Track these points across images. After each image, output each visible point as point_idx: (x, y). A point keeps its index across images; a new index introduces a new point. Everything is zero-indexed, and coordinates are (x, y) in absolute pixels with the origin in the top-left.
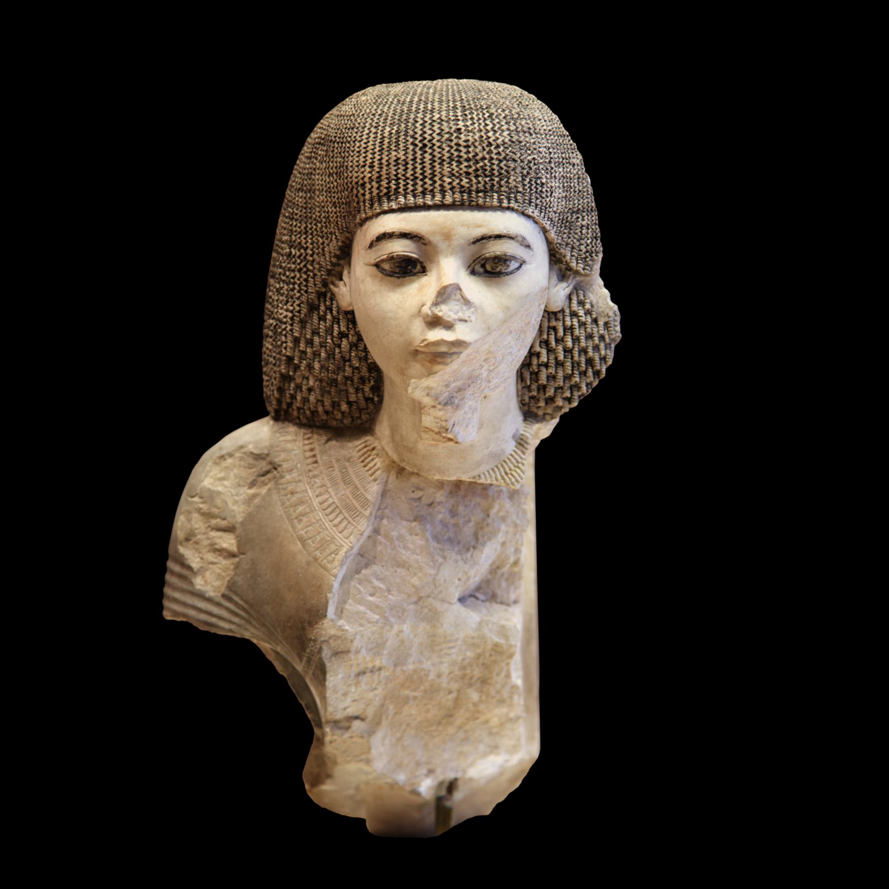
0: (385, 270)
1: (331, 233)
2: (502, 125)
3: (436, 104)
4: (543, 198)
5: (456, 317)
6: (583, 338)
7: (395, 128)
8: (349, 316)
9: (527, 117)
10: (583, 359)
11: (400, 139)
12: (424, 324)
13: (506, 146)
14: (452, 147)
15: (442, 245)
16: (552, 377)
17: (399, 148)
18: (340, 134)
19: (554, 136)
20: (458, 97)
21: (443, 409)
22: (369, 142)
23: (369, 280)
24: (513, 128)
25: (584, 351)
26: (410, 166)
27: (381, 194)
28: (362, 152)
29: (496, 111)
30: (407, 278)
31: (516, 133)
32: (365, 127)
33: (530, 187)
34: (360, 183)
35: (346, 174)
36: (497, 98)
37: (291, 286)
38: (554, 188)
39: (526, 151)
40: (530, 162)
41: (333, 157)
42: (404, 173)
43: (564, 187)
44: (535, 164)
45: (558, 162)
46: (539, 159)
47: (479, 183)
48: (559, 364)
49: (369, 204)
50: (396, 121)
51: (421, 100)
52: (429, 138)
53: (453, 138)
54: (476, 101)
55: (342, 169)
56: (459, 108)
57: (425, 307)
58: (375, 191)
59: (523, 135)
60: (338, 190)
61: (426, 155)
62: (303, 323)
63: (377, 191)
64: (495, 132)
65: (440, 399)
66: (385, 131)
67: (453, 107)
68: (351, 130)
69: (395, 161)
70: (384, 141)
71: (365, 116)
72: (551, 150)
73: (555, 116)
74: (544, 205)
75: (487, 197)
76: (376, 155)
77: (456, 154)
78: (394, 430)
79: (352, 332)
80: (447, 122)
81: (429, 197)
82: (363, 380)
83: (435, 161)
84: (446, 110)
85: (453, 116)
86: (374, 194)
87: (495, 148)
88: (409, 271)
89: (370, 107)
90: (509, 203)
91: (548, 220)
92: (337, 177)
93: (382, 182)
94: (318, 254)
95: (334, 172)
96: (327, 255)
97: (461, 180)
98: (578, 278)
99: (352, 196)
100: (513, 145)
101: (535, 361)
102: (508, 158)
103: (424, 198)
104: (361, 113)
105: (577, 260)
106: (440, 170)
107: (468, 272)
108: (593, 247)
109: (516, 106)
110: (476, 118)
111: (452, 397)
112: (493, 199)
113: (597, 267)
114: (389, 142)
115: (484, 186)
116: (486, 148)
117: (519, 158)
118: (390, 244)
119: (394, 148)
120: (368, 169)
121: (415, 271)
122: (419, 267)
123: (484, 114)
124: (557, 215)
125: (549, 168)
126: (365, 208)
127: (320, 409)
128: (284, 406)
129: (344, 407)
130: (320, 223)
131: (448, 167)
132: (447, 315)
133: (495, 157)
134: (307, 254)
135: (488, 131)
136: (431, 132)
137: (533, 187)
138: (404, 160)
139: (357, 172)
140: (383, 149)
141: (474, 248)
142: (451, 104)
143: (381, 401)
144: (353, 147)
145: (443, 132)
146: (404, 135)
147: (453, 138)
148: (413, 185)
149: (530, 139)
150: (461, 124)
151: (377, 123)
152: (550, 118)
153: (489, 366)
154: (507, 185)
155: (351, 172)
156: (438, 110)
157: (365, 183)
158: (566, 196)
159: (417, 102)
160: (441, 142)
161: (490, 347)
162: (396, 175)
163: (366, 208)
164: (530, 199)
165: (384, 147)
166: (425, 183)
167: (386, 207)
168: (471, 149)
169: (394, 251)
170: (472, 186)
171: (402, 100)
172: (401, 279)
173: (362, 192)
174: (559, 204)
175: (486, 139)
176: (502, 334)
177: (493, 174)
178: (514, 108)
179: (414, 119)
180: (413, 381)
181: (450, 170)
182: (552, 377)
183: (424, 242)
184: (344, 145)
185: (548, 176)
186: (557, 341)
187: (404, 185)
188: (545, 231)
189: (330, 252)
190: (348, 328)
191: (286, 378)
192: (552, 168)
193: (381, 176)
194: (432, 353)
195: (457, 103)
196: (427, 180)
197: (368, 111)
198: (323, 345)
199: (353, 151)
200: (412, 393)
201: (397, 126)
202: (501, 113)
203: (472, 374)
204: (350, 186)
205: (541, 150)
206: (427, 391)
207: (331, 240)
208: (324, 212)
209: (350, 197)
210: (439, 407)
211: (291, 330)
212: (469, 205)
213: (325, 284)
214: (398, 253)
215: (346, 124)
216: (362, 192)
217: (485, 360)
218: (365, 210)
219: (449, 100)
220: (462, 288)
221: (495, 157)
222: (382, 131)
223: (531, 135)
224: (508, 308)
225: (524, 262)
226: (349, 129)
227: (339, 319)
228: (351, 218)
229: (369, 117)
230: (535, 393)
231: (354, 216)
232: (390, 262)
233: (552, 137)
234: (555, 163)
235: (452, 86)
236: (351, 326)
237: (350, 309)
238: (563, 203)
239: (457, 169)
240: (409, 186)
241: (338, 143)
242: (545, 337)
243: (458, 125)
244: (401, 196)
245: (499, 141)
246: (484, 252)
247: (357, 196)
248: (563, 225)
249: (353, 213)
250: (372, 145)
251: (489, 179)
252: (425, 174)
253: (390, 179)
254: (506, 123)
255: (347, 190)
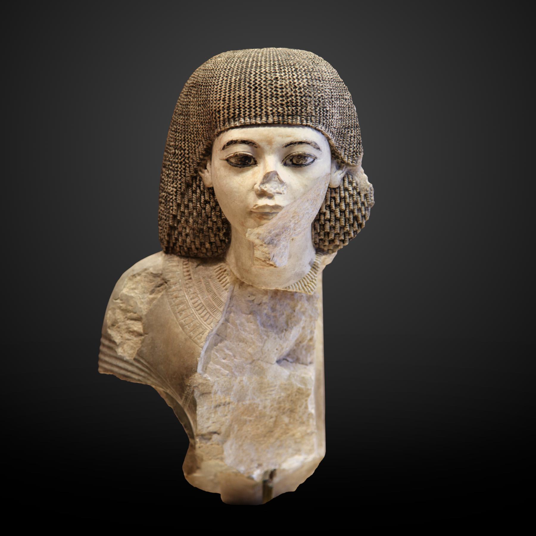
0: (232, 163)
1: (200, 141)
2: (303, 76)
3: (263, 63)
4: (328, 119)
5: (275, 191)
6: (351, 204)
7: (238, 77)
8: (211, 191)
9: (318, 70)
10: (352, 217)
11: (241, 84)
12: (255, 196)
13: (305, 88)
14: (272, 89)
15: (267, 148)
16: (333, 228)
17: (241, 89)
18: (205, 81)
19: (334, 82)
20: (276, 59)
21: (267, 247)
22: (222, 86)
23: (222, 169)
24: (309, 77)
25: (352, 212)
26: (247, 100)
27: (230, 117)
28: (218, 92)
29: (299, 67)
30: (246, 168)
31: (311, 80)
32: (220, 76)
33: (319, 113)
34: (217, 110)
35: (208, 105)
36: (300, 59)
37: (176, 173)
38: (334, 114)
39: (317, 91)
40: (319, 98)
41: (201, 95)
42: (243, 104)
43: (340, 113)
44: (322, 99)
45: (337, 98)
46: (325, 96)
47: (289, 110)
48: (337, 219)
49: (222, 123)
50: (239, 73)
51: (254, 60)
52: (259, 83)
53: (273, 83)
54: (287, 61)
55: (206, 102)
56: (277, 65)
57: (256, 185)
58: (226, 115)
59: (315, 81)
60: (204, 115)
61: (257, 94)
62: (183, 195)
63: (227, 115)
64: (299, 79)
65: (266, 241)
66: (232, 79)
67: (273, 65)
68: (211, 78)
69: (238, 97)
70: (231, 85)
71: (220, 70)
72: (332, 91)
73: (334, 70)
74: (328, 123)
75: (294, 119)
76: (227, 94)
77: (275, 93)
78: (238, 259)
79: (212, 200)
80: (269, 73)
81: (258, 119)
82: (219, 229)
83: (262, 97)
84: (269, 66)
85: (273, 70)
86: (226, 117)
87: (299, 89)
88: (246, 164)
89: (223, 65)
90: (307, 122)
91: (330, 133)
92: (203, 107)
93: (231, 110)
94: (192, 153)
95: (201, 104)
96: (197, 154)
97: (278, 109)
98: (349, 168)
99: (212, 118)
100: (309, 87)
101: (322, 218)
102: (306, 95)
103: (255, 119)
104: (218, 68)
105: (348, 157)
106: (265, 102)
107: (282, 164)
108: (357, 149)
109: (311, 64)
110: (287, 71)
111: (273, 239)
112: (297, 120)
113: (360, 161)
114: (234, 86)
115: (292, 112)
116: (293, 89)
117: (313, 95)
118: (235, 147)
119: (238, 89)
120: (222, 102)
121: (250, 164)
122: (252, 161)
123: (292, 69)
124: (336, 129)
125: (331, 101)
126: (220, 125)
127: (193, 247)
128: (171, 245)
129: (208, 245)
130: (193, 134)
131: (270, 101)
132: (269, 190)
133: (298, 95)
134: (185, 153)
135: (294, 79)
136: (260, 80)
137: (321, 113)
138: (244, 96)
139: (215, 104)
140: (231, 90)
141: (286, 149)
142: (272, 63)
143: (230, 242)
144: (213, 89)
145: (267, 80)
146: (243, 81)
147: (273, 83)
148: (249, 112)
149: (319, 84)
150: (278, 75)
151: (227, 74)
152: (332, 71)
153: (295, 221)
154: (305, 111)
155: (212, 104)
156: (264, 66)
157: (220, 110)
158: (341, 118)
159: (252, 61)
160: (266, 86)
161: (295, 209)
162: (239, 106)
163: (221, 125)
164: (320, 120)
165: (232, 88)
166: (256, 110)
167: (232, 125)
168: (284, 90)
169: (238, 151)
170: (284, 112)
171: (243, 60)
172: (242, 168)
173: (218, 116)
174: (337, 123)
175: (293, 84)
176: (303, 201)
177: (297, 105)
178: (310, 65)
179: (250, 71)
180: (249, 229)
181: (271, 102)
182: (333, 228)
183: (256, 146)
184: (207, 87)
185: (330, 106)
186: (336, 205)
187: (244, 112)
188: (328, 139)
189: (199, 152)
190: (210, 198)
191: (172, 228)
192: (333, 101)
193: (230, 106)
194: (260, 213)
195: (275, 62)
196: (257, 109)
197: (222, 67)
198: (194, 208)
199: (213, 91)
200: (248, 237)
201: (239, 76)
202: (302, 68)
203: (285, 226)
204: (211, 112)
205: (326, 90)
206: (257, 236)
207: (200, 145)
208: (196, 128)
209: (211, 119)
210: (265, 245)
211: (176, 199)
212: (283, 124)
213: (196, 171)
214: (240, 153)
215: (209, 75)
216: (218, 116)
217: (292, 217)
218: (220, 127)
219: (271, 60)
220: (279, 173)
221: (298, 95)
222: (230, 79)
223: (320, 81)
224: (306, 186)
225: (316, 158)
226: (210, 78)
227: (204, 192)
228: (211, 132)
229: (222, 70)
230: (322, 237)
231: (214, 130)
232: (235, 158)
233: (333, 83)
234: (335, 99)
235: (273, 52)
236: (211, 197)
237: (211, 186)
238: (340, 122)
239: (275, 102)
240: (247, 112)
241: (204, 86)
242: (329, 203)
243: (276, 75)
244: (241, 118)
245: (301, 85)
246: (292, 152)
247: (215, 118)
248: (339, 136)
249: (213, 128)
250: (225, 87)
251: (295, 108)
252: (257, 105)
253: (235, 108)
254: (305, 74)
255: (209, 115)
